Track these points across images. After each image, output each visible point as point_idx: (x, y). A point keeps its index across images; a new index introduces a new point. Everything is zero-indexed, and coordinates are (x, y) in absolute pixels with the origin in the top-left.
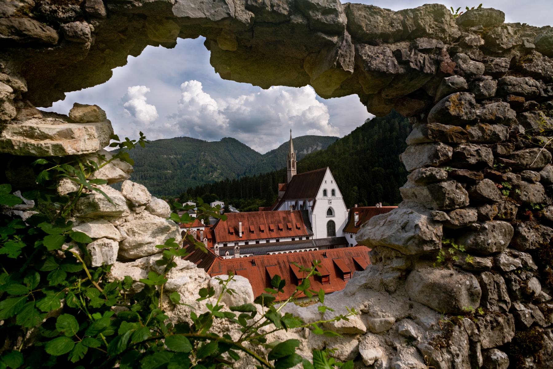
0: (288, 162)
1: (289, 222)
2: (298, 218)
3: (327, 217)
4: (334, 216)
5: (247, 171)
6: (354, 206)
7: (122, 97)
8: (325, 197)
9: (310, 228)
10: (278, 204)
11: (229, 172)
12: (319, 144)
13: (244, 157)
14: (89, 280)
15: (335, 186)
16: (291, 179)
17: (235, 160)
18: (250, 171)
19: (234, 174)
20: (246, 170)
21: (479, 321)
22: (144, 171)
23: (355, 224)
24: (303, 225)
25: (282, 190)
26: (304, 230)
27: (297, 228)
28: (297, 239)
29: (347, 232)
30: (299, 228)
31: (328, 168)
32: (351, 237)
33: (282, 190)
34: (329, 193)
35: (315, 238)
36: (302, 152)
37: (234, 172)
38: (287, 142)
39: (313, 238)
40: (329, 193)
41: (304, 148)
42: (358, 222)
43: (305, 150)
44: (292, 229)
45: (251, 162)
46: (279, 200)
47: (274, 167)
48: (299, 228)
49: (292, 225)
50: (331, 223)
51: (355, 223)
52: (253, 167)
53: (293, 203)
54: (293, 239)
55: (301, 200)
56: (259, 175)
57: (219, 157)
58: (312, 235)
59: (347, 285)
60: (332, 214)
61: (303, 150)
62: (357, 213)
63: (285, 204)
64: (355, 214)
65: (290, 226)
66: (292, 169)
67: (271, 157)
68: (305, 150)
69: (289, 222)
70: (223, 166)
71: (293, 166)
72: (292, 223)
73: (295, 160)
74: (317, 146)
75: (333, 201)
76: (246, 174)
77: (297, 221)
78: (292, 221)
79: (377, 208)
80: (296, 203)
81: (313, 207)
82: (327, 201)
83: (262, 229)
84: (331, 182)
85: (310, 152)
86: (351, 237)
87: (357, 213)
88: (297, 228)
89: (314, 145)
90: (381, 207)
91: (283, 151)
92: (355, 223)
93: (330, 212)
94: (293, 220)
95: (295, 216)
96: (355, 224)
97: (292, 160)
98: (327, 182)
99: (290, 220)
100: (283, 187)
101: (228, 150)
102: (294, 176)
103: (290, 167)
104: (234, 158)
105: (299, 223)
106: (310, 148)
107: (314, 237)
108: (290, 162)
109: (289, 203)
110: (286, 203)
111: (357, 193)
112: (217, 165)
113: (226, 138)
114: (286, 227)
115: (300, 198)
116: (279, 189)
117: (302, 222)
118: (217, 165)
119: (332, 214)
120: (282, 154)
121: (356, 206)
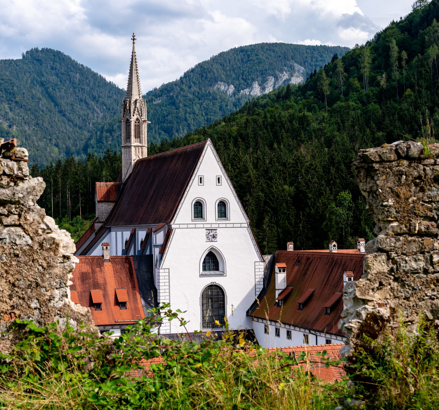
0: (123, 125)
1: (96, 286)
2: (124, 277)
3: (201, 276)
4: (223, 274)
5: (93, 141)
6: (285, 248)
8: (199, 222)
10: (93, 236)
11: (42, 144)
12: (297, 66)
13: (87, 103)
16: (130, 171)
17: (60, 112)
18: (99, 141)
19: (56, 150)
20: (89, 139)
23: (277, 296)
24: (134, 295)
25: (106, 199)
26: (136, 309)
27: (117, 303)
29: (258, 318)
30: (123, 305)
31: (209, 142)
32: (266, 331)
33: (106, 199)
35: (168, 332)
36: (247, 91)
37: (57, 145)
38: (205, 62)
39: (162, 332)
41: (253, 80)
42: (284, 291)
43: (256, 85)
44: (103, 306)
45: (105, 117)
46: (97, 226)
47: (168, 131)
48: (123, 305)
49: (105, 296)
50: (215, 291)
51: (277, 293)
52: (108, 131)
55: (142, 229)
56: (102, 155)
57: (16, 102)
60: (217, 268)
61: (249, 86)
62: (284, 265)
63: (110, 238)
64: (277, 270)
65: (97, 296)
66: (134, 142)
67: (160, 105)
68: (256, 85)
69: (96, 286)
70: (26, 128)
71: (138, 135)
72: (105, 290)
73: (145, 117)
74: (292, 73)
76: (90, 150)
77: (121, 284)
78: (105, 284)
79: (331, 253)
80: (133, 236)
81: (163, 248)
82: (204, 232)
83: (120, 300)
84: (215, 180)
85: (269, 90)
86: (266, 331)
87: (284, 265)
88: (117, 303)
89: (281, 71)
90: (335, 251)
91: (195, 88)
92: (277, 293)
94: (108, 280)
95: (116, 271)
96: (277, 296)
97: (133, 119)
98: (205, 180)
99: (101, 281)
100: (109, 192)
101: (42, 84)
102: (140, 162)
103: (128, 137)
104: (56, 104)
105: (125, 291)
106: (271, 81)
108: (128, 122)
109: (119, 233)
110: (113, 234)
111: (349, 209)
112: (10, 126)
113: (36, 50)
114: (88, 298)
116: (98, 197)
117: (134, 287)
118: (10, 126)
119: (217, 268)
120: (191, 96)
121: (290, 247)
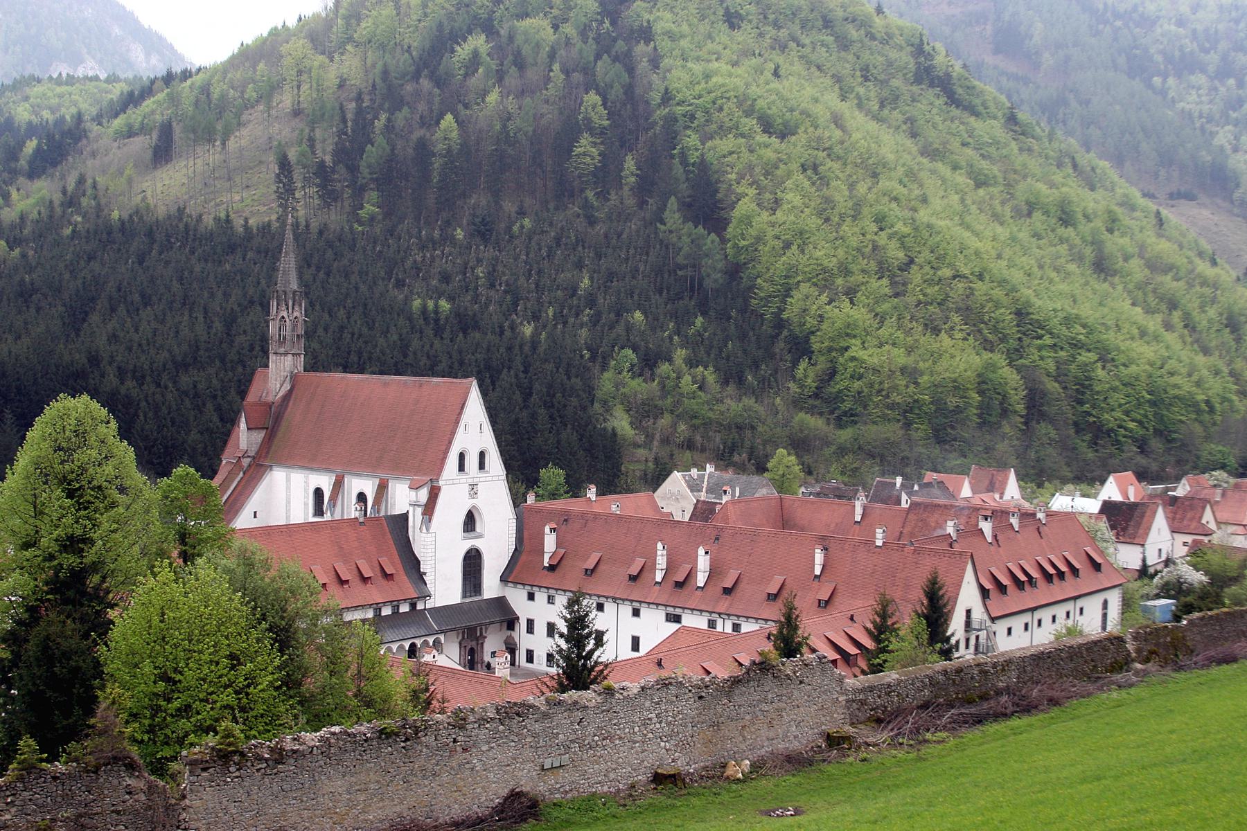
4: (481, 536)
7: (174, 71)
8: (462, 476)
9: (420, 577)
14: (1215, 414)
15: (488, 441)
21: (1088, 151)
22: (560, 416)
28: (404, 608)
34: (472, 462)
40: (472, 462)
53: (325, 482)
54: (378, 610)
58: (426, 596)
59: (1202, 284)
75: (481, 488)
82: (467, 488)
86: (531, 597)
93: (470, 522)
107: (430, 604)
115: (361, 468)
